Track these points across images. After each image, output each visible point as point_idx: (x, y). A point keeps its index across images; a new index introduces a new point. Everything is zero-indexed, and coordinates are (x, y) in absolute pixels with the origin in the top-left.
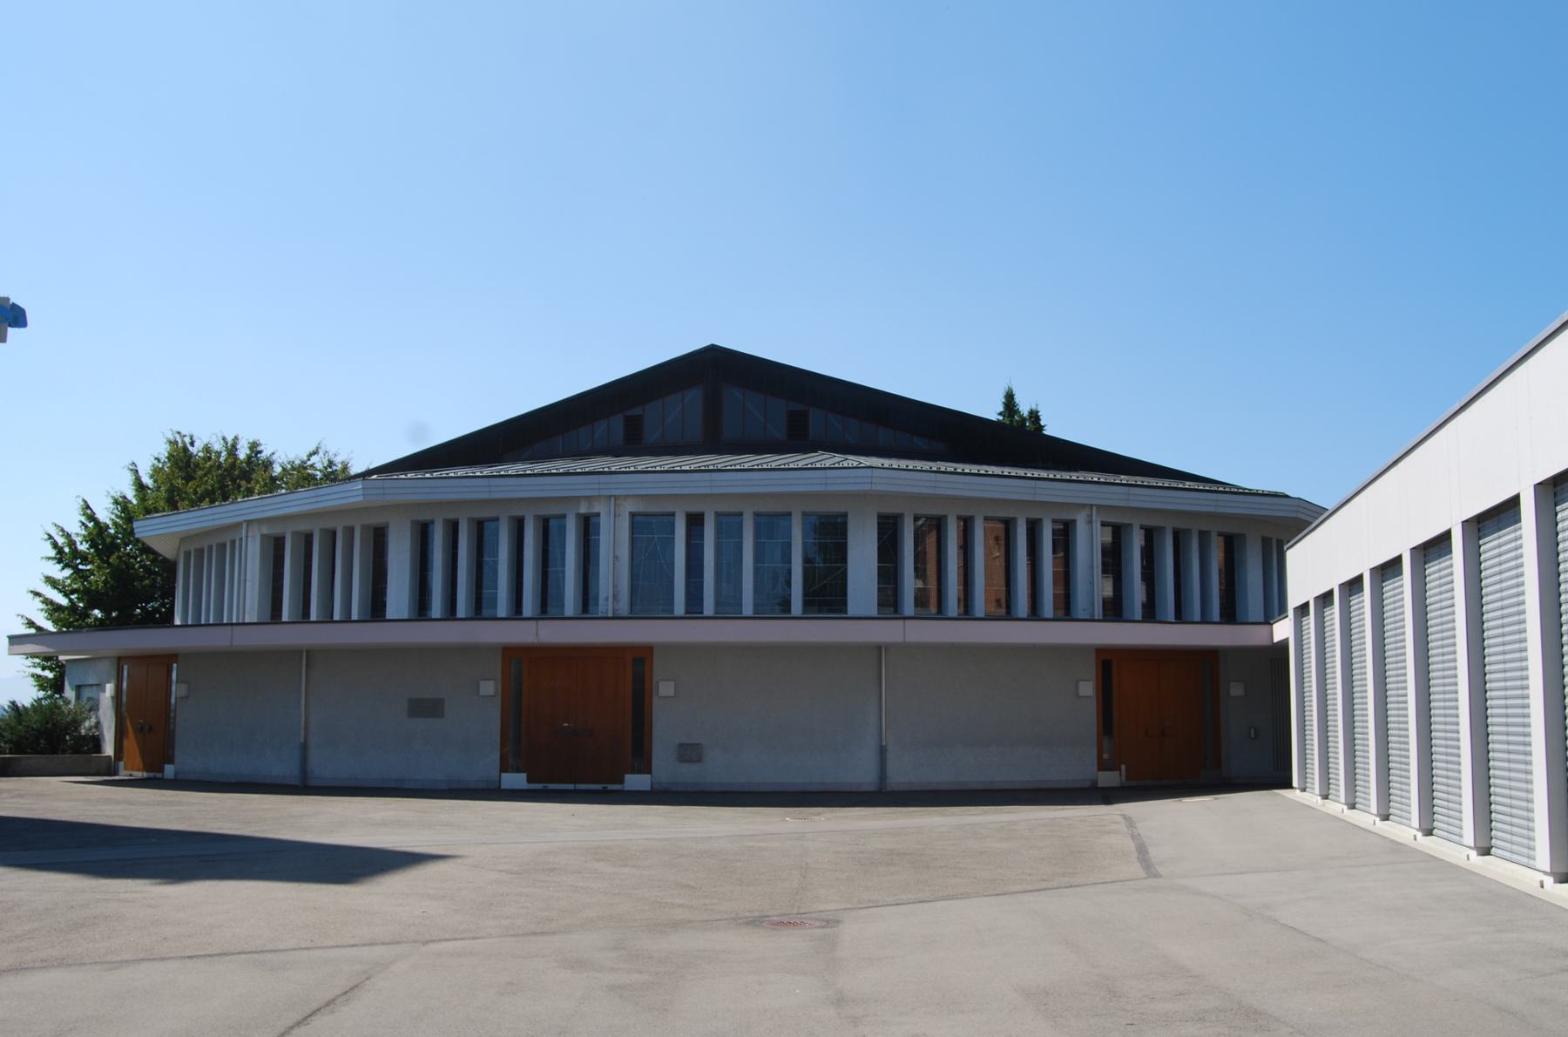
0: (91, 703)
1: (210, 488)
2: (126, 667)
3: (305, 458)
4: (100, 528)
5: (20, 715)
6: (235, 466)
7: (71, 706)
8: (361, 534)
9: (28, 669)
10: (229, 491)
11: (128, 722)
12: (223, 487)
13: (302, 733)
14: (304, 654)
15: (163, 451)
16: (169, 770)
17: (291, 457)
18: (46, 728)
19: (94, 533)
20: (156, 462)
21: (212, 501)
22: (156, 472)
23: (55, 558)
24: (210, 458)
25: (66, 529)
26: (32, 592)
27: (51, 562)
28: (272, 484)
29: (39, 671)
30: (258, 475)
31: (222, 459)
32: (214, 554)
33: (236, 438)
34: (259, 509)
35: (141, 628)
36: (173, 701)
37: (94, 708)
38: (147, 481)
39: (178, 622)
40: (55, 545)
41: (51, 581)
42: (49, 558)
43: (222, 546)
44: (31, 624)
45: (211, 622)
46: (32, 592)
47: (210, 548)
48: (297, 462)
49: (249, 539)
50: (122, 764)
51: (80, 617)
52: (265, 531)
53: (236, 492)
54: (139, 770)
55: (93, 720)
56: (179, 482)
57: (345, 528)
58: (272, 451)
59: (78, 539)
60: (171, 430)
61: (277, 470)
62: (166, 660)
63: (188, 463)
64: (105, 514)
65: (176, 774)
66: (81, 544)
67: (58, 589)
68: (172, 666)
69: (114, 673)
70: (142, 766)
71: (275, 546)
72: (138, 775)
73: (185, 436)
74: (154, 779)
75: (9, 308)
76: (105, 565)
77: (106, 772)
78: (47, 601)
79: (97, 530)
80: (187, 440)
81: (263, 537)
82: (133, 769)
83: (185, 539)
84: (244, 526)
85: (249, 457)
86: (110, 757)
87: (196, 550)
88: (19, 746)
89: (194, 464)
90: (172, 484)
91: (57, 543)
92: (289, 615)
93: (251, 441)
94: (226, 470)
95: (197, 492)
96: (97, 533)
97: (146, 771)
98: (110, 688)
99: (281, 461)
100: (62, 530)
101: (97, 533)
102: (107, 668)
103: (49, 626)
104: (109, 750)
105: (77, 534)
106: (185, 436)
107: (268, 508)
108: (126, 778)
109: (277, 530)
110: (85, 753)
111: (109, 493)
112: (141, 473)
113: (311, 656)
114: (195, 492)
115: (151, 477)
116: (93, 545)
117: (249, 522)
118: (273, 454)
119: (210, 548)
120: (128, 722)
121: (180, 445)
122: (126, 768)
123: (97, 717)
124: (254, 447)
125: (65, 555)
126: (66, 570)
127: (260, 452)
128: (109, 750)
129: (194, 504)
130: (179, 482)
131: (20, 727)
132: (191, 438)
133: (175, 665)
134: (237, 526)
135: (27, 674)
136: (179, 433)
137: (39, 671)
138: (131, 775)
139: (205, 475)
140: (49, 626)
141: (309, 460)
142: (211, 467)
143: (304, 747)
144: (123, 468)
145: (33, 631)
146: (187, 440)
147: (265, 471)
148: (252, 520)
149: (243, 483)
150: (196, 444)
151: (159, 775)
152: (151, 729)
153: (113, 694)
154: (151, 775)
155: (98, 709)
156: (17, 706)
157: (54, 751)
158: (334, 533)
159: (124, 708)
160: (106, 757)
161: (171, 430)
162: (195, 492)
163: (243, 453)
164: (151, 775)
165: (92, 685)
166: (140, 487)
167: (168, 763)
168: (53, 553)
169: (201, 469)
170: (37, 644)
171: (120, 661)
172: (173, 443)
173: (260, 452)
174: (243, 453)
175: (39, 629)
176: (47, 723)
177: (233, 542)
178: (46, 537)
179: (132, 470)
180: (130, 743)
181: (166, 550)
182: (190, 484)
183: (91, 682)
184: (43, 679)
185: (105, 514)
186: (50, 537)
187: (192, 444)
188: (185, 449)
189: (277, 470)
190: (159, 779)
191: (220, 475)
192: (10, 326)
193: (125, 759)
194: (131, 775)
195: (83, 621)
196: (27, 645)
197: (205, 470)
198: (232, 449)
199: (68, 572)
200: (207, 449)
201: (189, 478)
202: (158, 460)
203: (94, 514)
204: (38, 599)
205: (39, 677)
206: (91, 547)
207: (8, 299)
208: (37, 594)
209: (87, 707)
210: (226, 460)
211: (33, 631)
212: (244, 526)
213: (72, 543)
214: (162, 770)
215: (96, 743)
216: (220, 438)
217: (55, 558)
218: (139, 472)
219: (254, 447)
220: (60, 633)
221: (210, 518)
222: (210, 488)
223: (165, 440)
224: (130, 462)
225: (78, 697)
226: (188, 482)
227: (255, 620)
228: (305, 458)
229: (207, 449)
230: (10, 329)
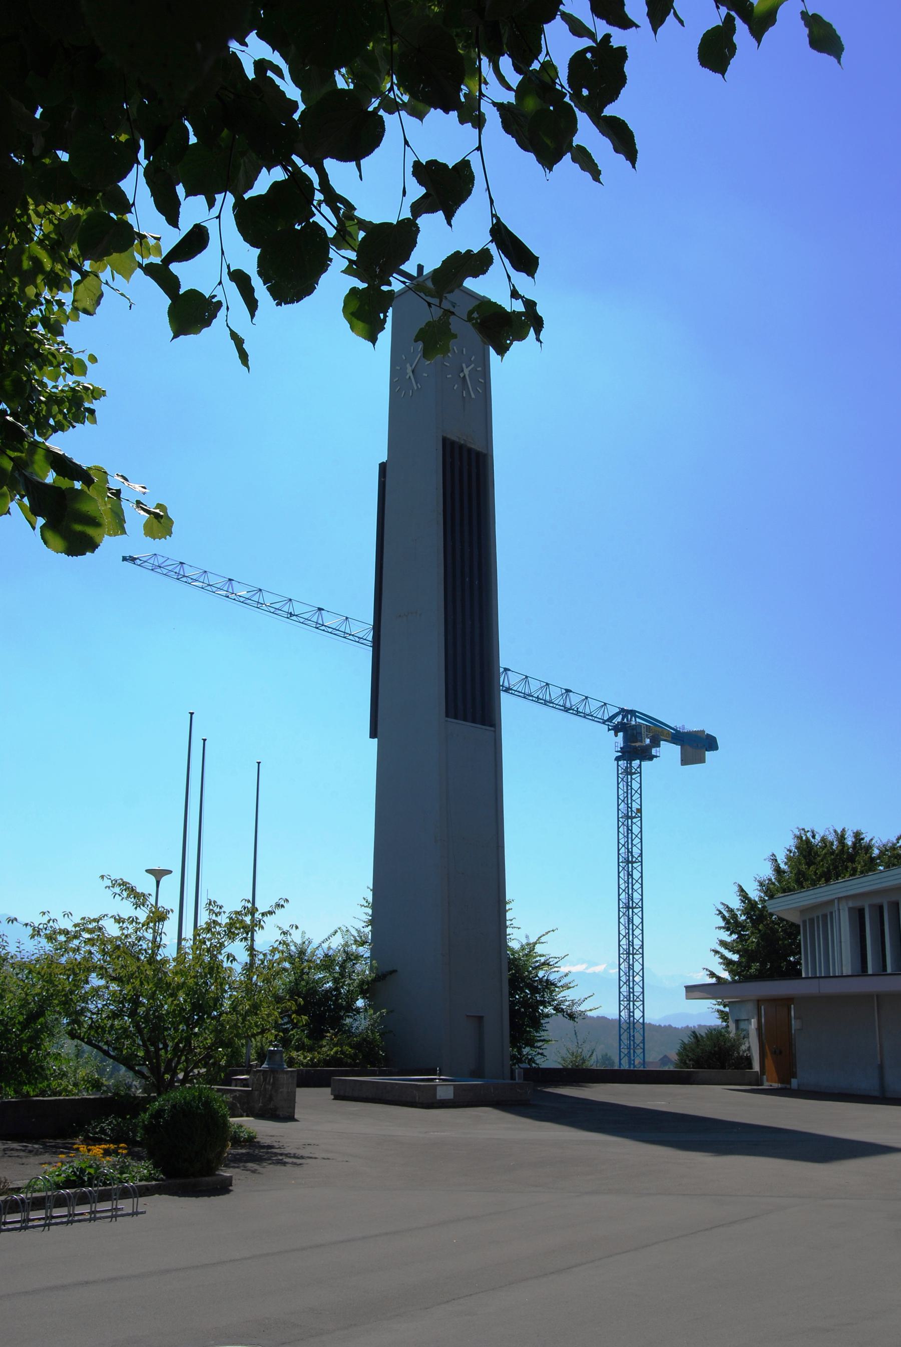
0: (744, 1033)
1: (826, 870)
2: (763, 1007)
3: (895, 841)
4: (752, 904)
5: (698, 1041)
6: (843, 851)
7: (732, 1035)
8: (889, 915)
9: (713, 1006)
10: (839, 871)
11: (767, 1047)
12: (836, 867)
13: (879, 1057)
14: (875, 998)
15: (791, 843)
16: (794, 1083)
17: (885, 841)
18: (714, 1051)
19: (749, 908)
20: (788, 853)
21: (827, 881)
22: (789, 859)
23: (723, 928)
24: (826, 846)
25: (731, 906)
26: (713, 950)
27: (722, 930)
28: (871, 864)
29: (721, 1008)
30: (862, 858)
31: (834, 847)
32: (821, 922)
33: (844, 830)
34: (843, 890)
35: (760, 981)
36: (793, 1032)
37: (747, 1036)
38: (783, 866)
39: (803, 975)
40: (724, 918)
41: (723, 943)
42: (720, 928)
43: (825, 916)
44: (712, 975)
45: (823, 975)
46: (713, 950)
47: (818, 917)
48: (890, 845)
49: (841, 911)
50: (765, 1077)
51: (745, 968)
52: (851, 904)
53: (845, 871)
54: (775, 1082)
55: (747, 1045)
56: (804, 867)
57: (889, 902)
58: (871, 838)
59: (739, 913)
60: (798, 828)
61: (876, 852)
62: (786, 1002)
63: (810, 853)
64: (754, 894)
65: (799, 1085)
66: (741, 916)
67: (728, 949)
68: (790, 1005)
69: (756, 1011)
70: (777, 1079)
71: (859, 915)
72: (776, 1085)
73: (808, 831)
74: (785, 1089)
75: (704, 737)
76: (756, 931)
77: (754, 1084)
78: (723, 957)
79: (750, 905)
80: (809, 835)
81: (850, 909)
82: (772, 1082)
83: (803, 911)
84: (836, 901)
85: (854, 844)
86: (758, 1072)
87: (809, 919)
88: (698, 1064)
89: (814, 852)
90: (799, 869)
91: (725, 916)
92: (873, 969)
93: (855, 831)
94: (837, 855)
95: (817, 874)
96: (750, 905)
97: (781, 1083)
98: (754, 1022)
99: (877, 845)
100: (728, 907)
101: (750, 905)
102: (751, 1007)
103: (725, 975)
104: (756, 1067)
105: (738, 910)
106: (808, 831)
107: (850, 888)
108: (767, 1087)
109: (858, 904)
110: (742, 1069)
111: (756, 878)
112: (779, 861)
113: (880, 998)
114: (816, 874)
115: (786, 864)
116: (749, 917)
117: (839, 899)
118: (872, 840)
119: (818, 917)
120: (767, 1047)
121: (804, 838)
122: (767, 1081)
123: (749, 1043)
124: (858, 836)
125: (731, 923)
126: (733, 935)
127: (863, 839)
128: (756, 1067)
129: (814, 884)
130: (804, 867)
131: (698, 1050)
132: (813, 833)
133: (792, 1006)
134: (832, 901)
135: (714, 1010)
136: (803, 829)
137: (721, 1008)
138: (771, 1086)
139: (822, 860)
140: (725, 975)
141: (898, 842)
142: (826, 854)
143: (881, 1067)
144: (765, 860)
145: (713, 980)
146: (809, 835)
147: (866, 854)
148: (841, 897)
149: (849, 864)
150: (816, 837)
151: (788, 1086)
152: (781, 1053)
153: (756, 1027)
154: (784, 1086)
155: (748, 1037)
156: (696, 1035)
157: (723, 1067)
158: (881, 908)
159: (764, 1037)
160: (755, 1072)
161: (798, 828)
162: (816, 874)
163: (849, 841)
164: (784, 1086)
165: (745, 1020)
166: (778, 871)
167: (793, 1078)
168: (723, 924)
169: (819, 856)
170: (702, 992)
171: (759, 1002)
172: (800, 838)
173: (863, 839)
174: (849, 841)
175: (718, 978)
176: (715, 1047)
177: (831, 913)
178: (718, 912)
179: (772, 860)
180: (769, 1062)
181: (794, 918)
182: (811, 868)
183: (744, 1018)
184: (725, 1014)
185: (754, 894)
186: (720, 913)
187: (814, 837)
188: (807, 840)
189: (876, 852)
190: (788, 1089)
191: (833, 859)
192: (707, 750)
193: (766, 1074)
194: (771, 1086)
195: (748, 971)
196: (696, 993)
197: (822, 856)
198: (841, 838)
199: (735, 936)
200: (823, 840)
201: (809, 864)
202: (791, 852)
203: (747, 894)
204: (717, 956)
205: (722, 1012)
206: (747, 918)
207: (703, 731)
208: (716, 952)
209: (742, 1035)
210: (837, 848)
211: (713, 980)
212: (836, 901)
213: (734, 916)
214: (789, 1083)
215: (748, 1062)
216: (832, 832)
217: (723, 928)
218: (778, 860)
219: (858, 836)
220: (734, 981)
221: (814, 896)
222: (826, 870)
223: (793, 837)
224: (771, 854)
225: (737, 1028)
226: (809, 867)
227: (850, 973)
228: (895, 841)
229: (823, 840)
230: (706, 752)
